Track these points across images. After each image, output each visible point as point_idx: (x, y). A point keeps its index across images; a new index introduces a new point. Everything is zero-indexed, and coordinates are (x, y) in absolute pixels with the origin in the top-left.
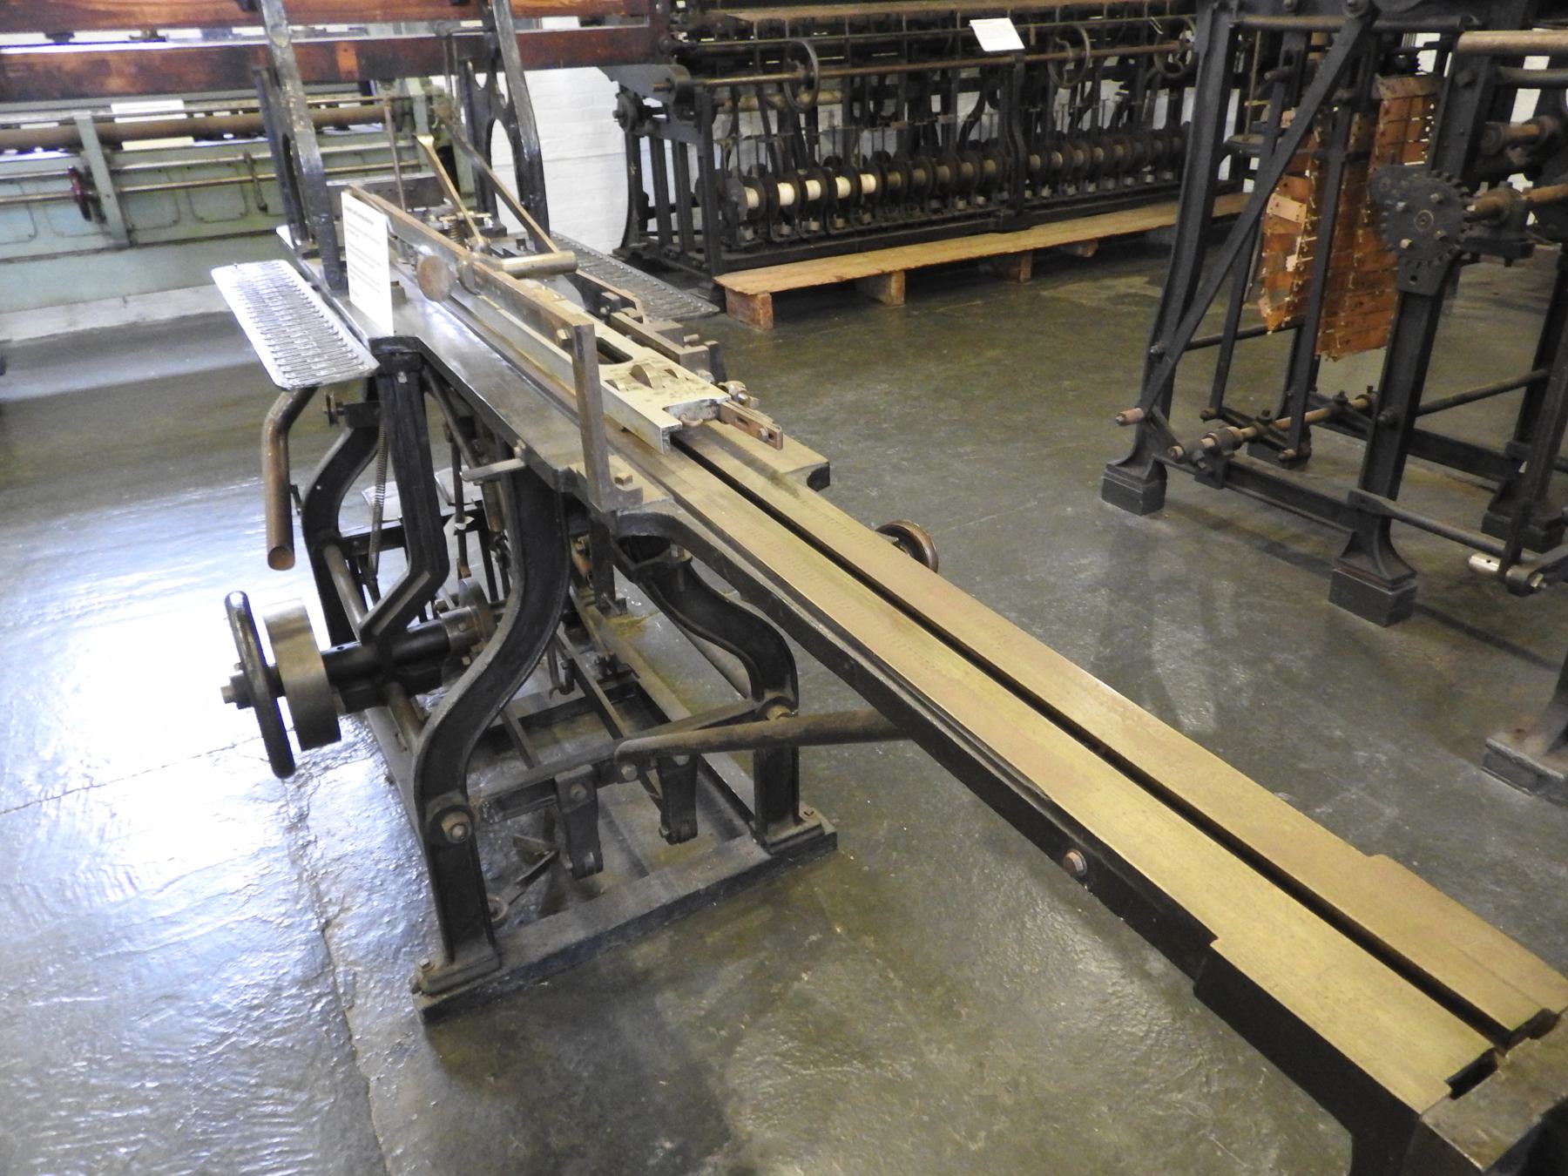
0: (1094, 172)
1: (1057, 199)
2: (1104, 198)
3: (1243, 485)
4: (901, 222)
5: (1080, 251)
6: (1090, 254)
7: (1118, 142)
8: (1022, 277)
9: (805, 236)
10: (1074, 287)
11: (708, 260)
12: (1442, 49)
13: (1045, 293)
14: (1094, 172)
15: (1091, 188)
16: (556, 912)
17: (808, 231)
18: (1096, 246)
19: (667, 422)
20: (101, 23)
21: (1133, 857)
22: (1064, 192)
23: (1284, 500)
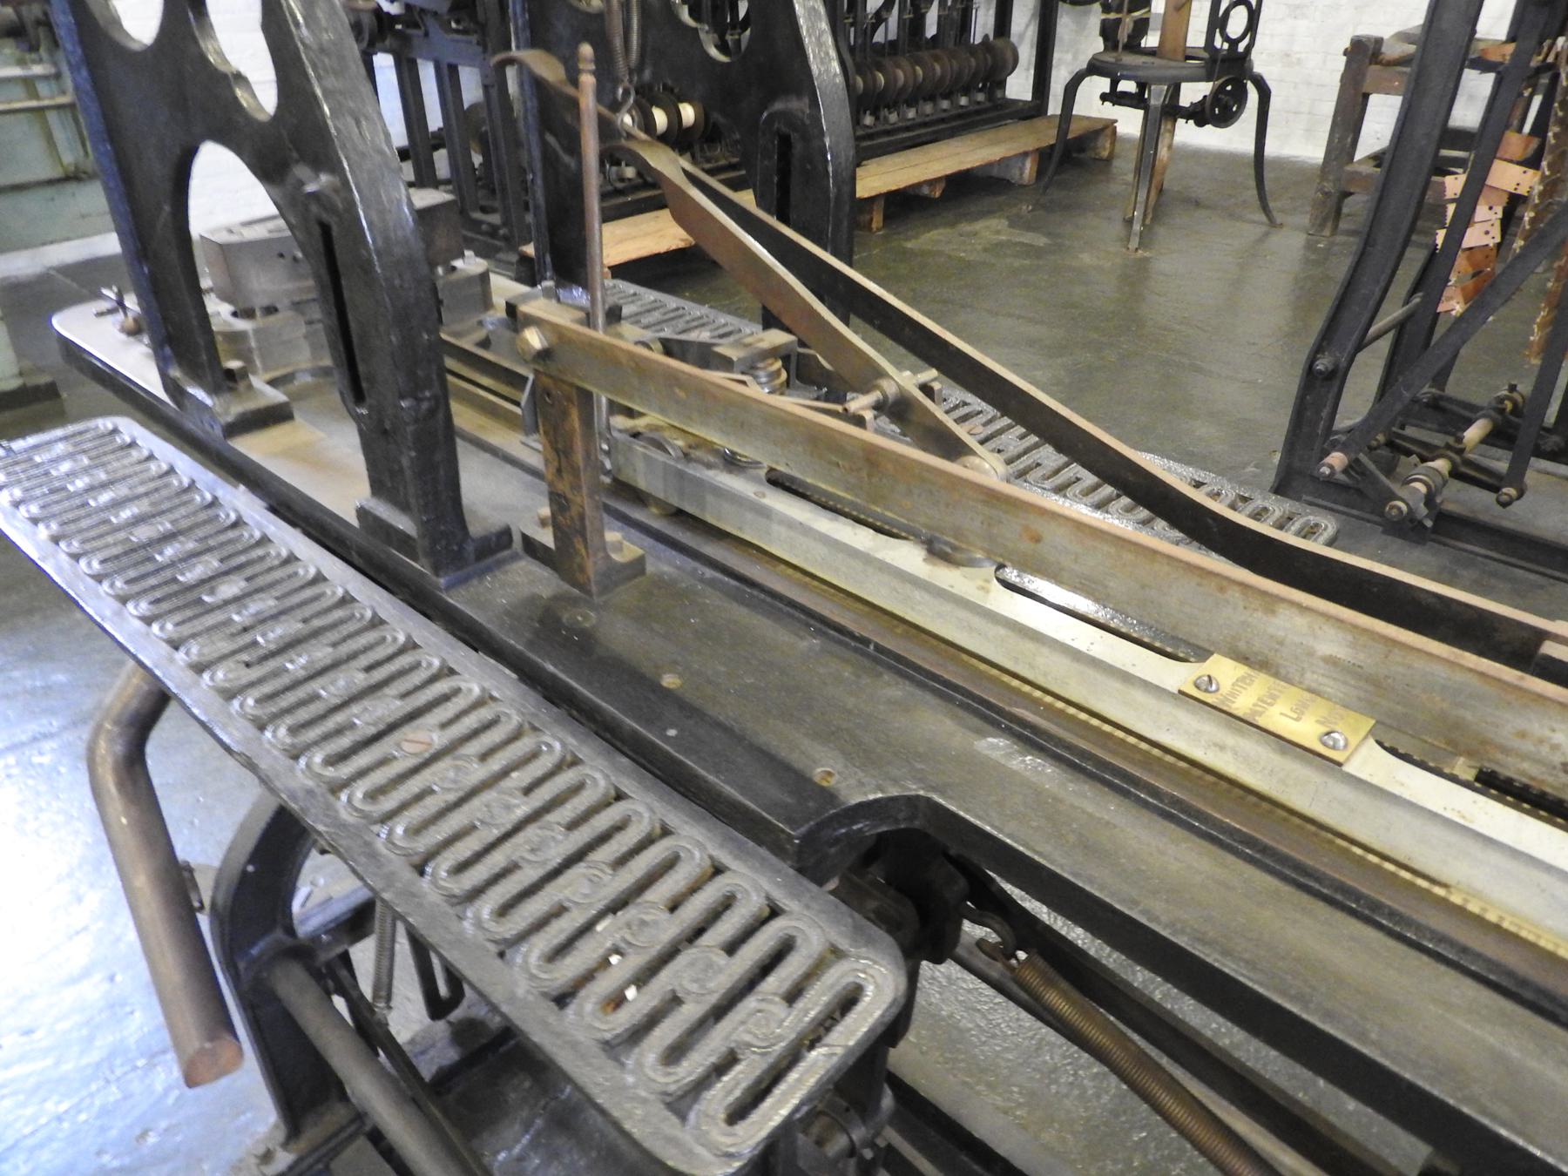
0: (914, 96)
1: (880, 128)
2: (925, 125)
3: (1458, 539)
4: (723, 162)
5: (926, 191)
6: (937, 195)
7: (937, 59)
8: (874, 226)
9: (620, 185)
10: (935, 234)
11: (505, 223)
12: (326, 30)
13: (909, 245)
14: (914, 96)
15: (911, 114)
16: (509, 1032)
17: (622, 180)
18: (943, 185)
19: (536, 436)
20: (634, 1155)
21: (1329, 1015)
22: (886, 119)
23: (1522, 558)
